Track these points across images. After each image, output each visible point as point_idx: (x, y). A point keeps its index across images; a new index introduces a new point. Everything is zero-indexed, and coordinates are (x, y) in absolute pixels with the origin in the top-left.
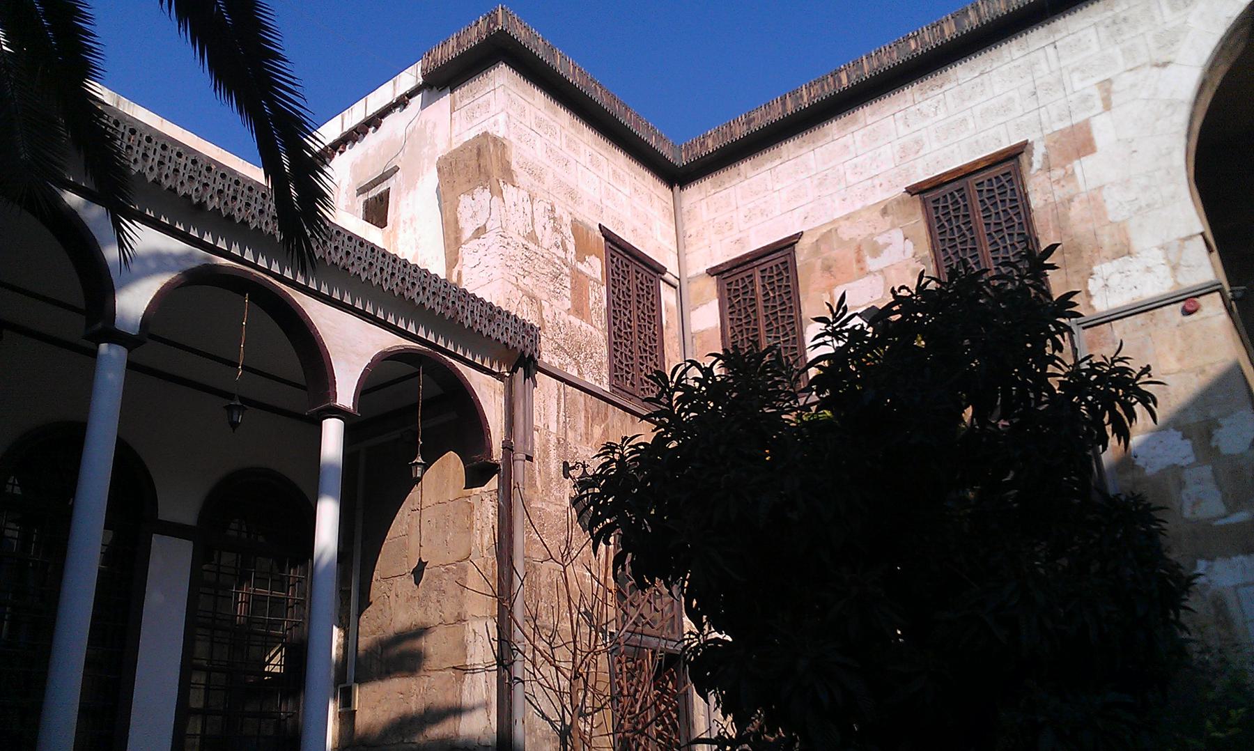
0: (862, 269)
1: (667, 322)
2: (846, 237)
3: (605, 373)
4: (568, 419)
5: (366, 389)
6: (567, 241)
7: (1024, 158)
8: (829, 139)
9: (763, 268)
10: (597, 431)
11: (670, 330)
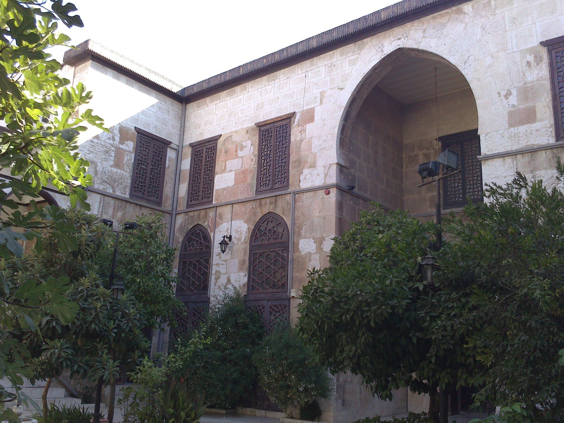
0: (236, 155)
1: (168, 165)
2: (234, 140)
4: (104, 211)
6: (115, 136)
7: (293, 119)
8: (236, 95)
9: (208, 147)
10: (119, 214)
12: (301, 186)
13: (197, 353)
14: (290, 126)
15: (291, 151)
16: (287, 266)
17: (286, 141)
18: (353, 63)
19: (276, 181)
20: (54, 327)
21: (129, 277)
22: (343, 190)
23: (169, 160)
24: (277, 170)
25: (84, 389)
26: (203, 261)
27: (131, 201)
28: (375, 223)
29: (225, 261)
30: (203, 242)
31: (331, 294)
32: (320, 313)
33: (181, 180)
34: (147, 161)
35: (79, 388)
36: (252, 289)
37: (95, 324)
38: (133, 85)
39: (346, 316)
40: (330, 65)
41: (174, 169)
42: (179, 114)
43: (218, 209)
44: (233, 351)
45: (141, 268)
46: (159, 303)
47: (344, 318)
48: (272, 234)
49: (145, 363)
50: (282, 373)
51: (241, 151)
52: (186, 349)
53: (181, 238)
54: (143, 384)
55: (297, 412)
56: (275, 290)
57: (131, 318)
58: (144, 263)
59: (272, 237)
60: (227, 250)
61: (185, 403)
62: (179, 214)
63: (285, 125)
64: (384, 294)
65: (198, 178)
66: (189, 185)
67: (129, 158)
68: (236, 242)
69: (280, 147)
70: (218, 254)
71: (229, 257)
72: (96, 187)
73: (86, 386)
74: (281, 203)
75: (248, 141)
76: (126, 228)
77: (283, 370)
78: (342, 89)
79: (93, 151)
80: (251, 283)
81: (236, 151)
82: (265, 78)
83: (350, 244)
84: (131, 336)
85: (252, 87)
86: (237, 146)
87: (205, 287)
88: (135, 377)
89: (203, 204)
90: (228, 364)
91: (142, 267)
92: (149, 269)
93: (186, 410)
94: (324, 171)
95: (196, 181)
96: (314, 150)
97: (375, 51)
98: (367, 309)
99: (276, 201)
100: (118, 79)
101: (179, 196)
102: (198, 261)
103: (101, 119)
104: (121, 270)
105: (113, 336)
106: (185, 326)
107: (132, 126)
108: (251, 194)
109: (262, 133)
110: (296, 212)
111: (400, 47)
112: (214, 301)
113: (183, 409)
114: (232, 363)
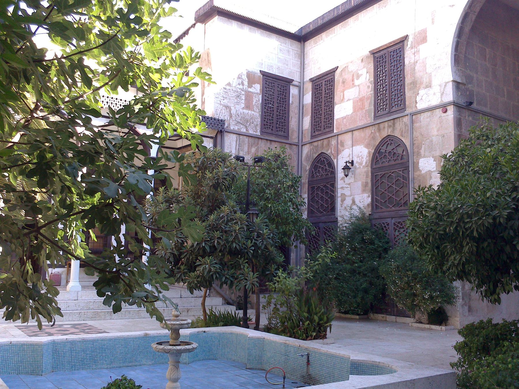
1: (292, 102)
2: (350, 70)
7: (406, 42)
9: (326, 80)
10: (253, 150)
11: (294, 105)
13: (329, 267)
15: (406, 74)
16: (408, 185)
17: (401, 64)
20: (204, 247)
21: (262, 203)
22: (461, 107)
23: (293, 97)
24: (393, 93)
25: (238, 298)
27: (262, 137)
28: (485, 138)
29: (349, 184)
30: (328, 168)
31: (435, 208)
32: (425, 227)
33: (304, 114)
35: (233, 297)
36: (376, 208)
37: (236, 243)
38: (255, 33)
39: (450, 228)
41: (297, 104)
42: (298, 52)
43: (340, 137)
44: (361, 264)
45: (271, 195)
46: (289, 224)
47: (447, 230)
48: (392, 155)
49: (280, 274)
50: (408, 283)
52: (314, 263)
53: (308, 166)
54: (281, 293)
55: (425, 318)
56: (397, 208)
57: (265, 238)
58: (273, 191)
59: (392, 159)
60: (350, 174)
61: (318, 309)
62: (305, 144)
63: (399, 49)
64: (484, 206)
65: (319, 110)
66: (312, 117)
68: (358, 166)
69: (395, 71)
70: (342, 179)
71: (352, 180)
72: (232, 128)
73: (239, 296)
74: (399, 125)
75: (363, 69)
76: (256, 162)
77: (408, 280)
78: (453, 6)
79: (227, 96)
80: (375, 203)
81: (353, 80)
83: (458, 160)
84: (267, 252)
86: (353, 75)
87: (333, 209)
88: (274, 286)
89: (325, 133)
90: (358, 276)
92: (278, 195)
93: (319, 315)
94: (440, 90)
96: (429, 70)
98: (468, 220)
99: (394, 124)
103: (209, 75)
104: (254, 198)
105: (251, 252)
106: (318, 243)
108: (370, 120)
110: (414, 133)
112: (341, 221)
113: (316, 314)
114: (362, 274)
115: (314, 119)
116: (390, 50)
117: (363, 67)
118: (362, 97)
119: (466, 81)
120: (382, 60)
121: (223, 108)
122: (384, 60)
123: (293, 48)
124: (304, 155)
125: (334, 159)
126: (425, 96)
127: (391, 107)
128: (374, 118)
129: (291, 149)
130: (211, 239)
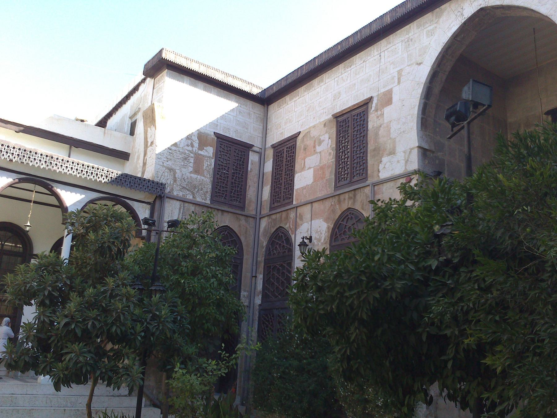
0: (314, 151)
1: (251, 169)
2: (312, 136)
3: (209, 196)
5: (469, 81)
6: (194, 143)
7: (370, 104)
8: (314, 89)
9: (287, 146)
11: (253, 172)
12: (380, 177)
14: (367, 113)
18: (431, 34)
19: (355, 174)
21: (174, 277)
24: (355, 161)
26: (285, 265)
27: (212, 206)
30: (285, 245)
33: (264, 183)
34: (228, 166)
37: (117, 326)
40: (406, 40)
41: (257, 172)
43: (299, 209)
44: (310, 360)
51: (319, 146)
53: (265, 242)
63: (363, 112)
65: (279, 179)
66: (271, 187)
67: (209, 163)
72: (175, 194)
79: (172, 158)
81: (314, 147)
82: (341, 66)
85: (328, 78)
86: (315, 141)
91: (189, 267)
94: (405, 157)
95: (278, 183)
96: (393, 136)
97: (454, 16)
99: (355, 196)
100: (195, 86)
101: (263, 200)
102: (281, 265)
107: (211, 132)
108: (330, 190)
109: (339, 124)
111: (481, 6)
115: (273, 189)
116: (354, 113)
117: (325, 132)
118: (323, 165)
119: (435, 148)
120: (345, 124)
121: (166, 170)
122: (347, 125)
123: (254, 111)
124: (262, 230)
125: (292, 234)
126: (388, 163)
127: (353, 176)
128: (334, 190)
129: (246, 221)
130: (84, 320)
